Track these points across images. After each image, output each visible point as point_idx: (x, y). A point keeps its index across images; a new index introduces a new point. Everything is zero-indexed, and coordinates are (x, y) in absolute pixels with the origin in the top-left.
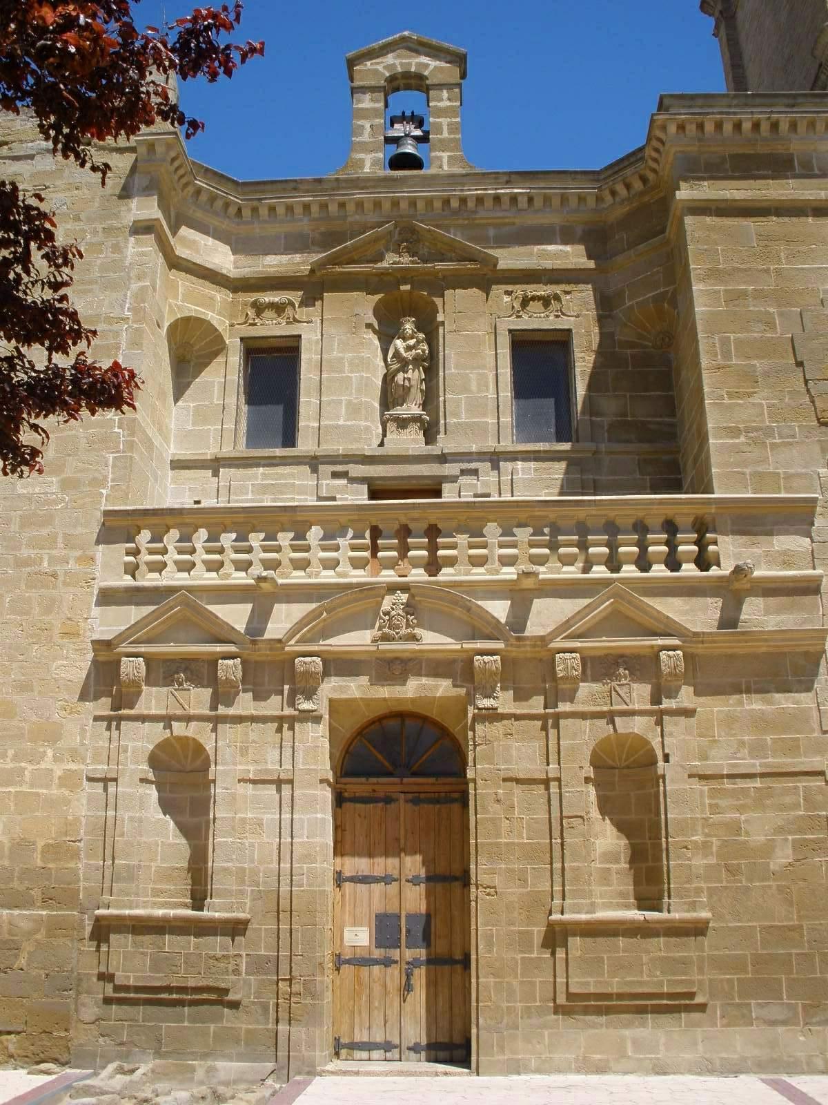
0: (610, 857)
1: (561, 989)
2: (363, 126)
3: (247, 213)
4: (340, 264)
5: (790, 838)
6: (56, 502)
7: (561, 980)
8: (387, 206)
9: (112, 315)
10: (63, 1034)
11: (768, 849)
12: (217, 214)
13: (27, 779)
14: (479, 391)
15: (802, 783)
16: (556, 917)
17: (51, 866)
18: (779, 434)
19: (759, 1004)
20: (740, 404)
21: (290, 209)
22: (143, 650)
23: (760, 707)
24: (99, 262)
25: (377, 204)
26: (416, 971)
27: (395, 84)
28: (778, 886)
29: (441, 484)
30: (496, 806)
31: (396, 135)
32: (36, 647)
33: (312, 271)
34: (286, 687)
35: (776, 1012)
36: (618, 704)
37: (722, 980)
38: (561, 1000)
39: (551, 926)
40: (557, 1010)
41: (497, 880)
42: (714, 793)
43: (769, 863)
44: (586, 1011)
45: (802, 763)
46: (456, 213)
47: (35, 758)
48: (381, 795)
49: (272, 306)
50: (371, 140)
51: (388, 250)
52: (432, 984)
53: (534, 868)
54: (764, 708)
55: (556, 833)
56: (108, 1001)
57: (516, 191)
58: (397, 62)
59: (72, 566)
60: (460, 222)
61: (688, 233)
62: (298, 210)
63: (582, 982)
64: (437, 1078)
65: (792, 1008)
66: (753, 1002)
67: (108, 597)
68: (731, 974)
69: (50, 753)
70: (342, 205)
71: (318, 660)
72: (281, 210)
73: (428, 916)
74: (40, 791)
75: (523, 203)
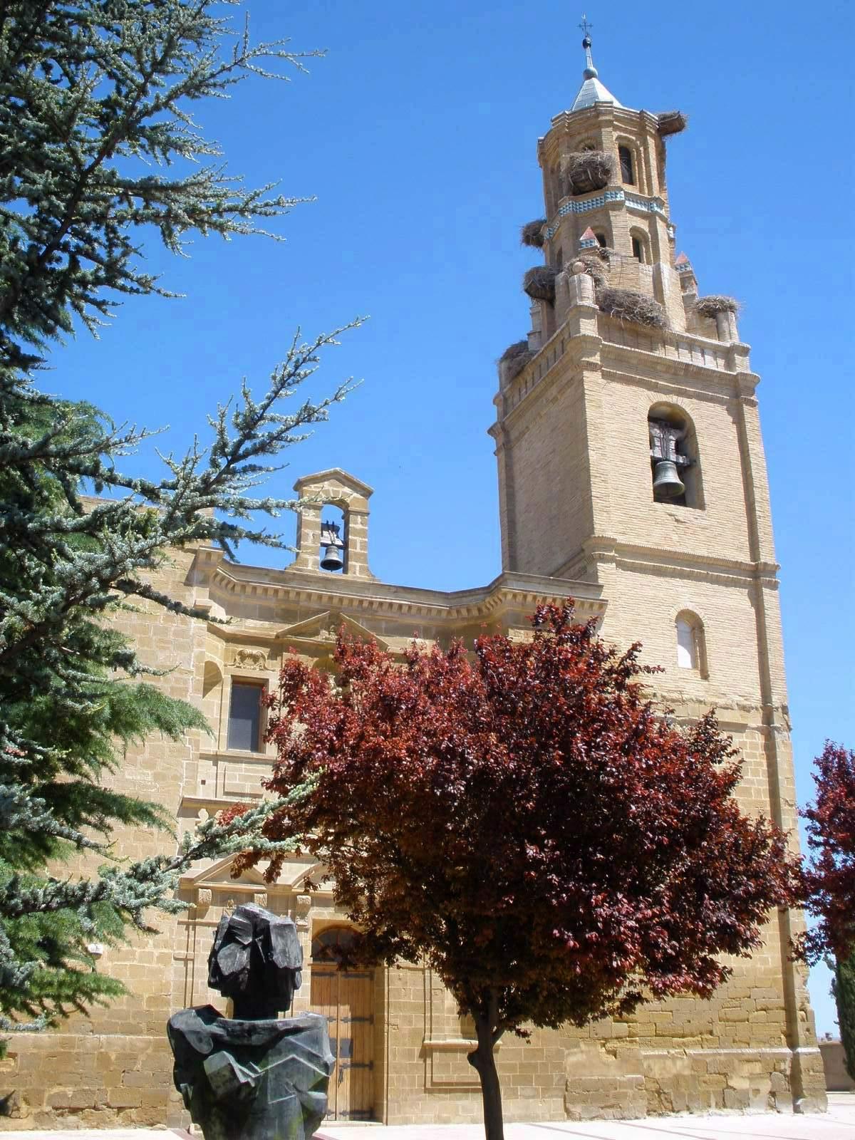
0: (450, 1011)
1: (428, 1080)
3: (238, 589)
4: (296, 635)
6: (151, 787)
7: (429, 1075)
8: (325, 600)
10: (164, 1108)
12: (221, 588)
16: (427, 1042)
22: (211, 885)
24: (173, 629)
25: (320, 597)
26: (345, 1071)
30: (399, 982)
33: (277, 637)
34: (290, 911)
35: (529, 1092)
38: (429, 1085)
39: (424, 1046)
40: (426, 1091)
41: (398, 1022)
44: (440, 1091)
46: (364, 610)
48: (329, 971)
49: (251, 656)
51: (322, 628)
52: (353, 1078)
55: (428, 996)
60: (367, 616)
62: (271, 593)
63: (439, 1076)
65: (537, 1090)
69: (151, 942)
70: (298, 594)
72: (259, 591)
73: (352, 1040)
74: (146, 965)
75: (405, 609)
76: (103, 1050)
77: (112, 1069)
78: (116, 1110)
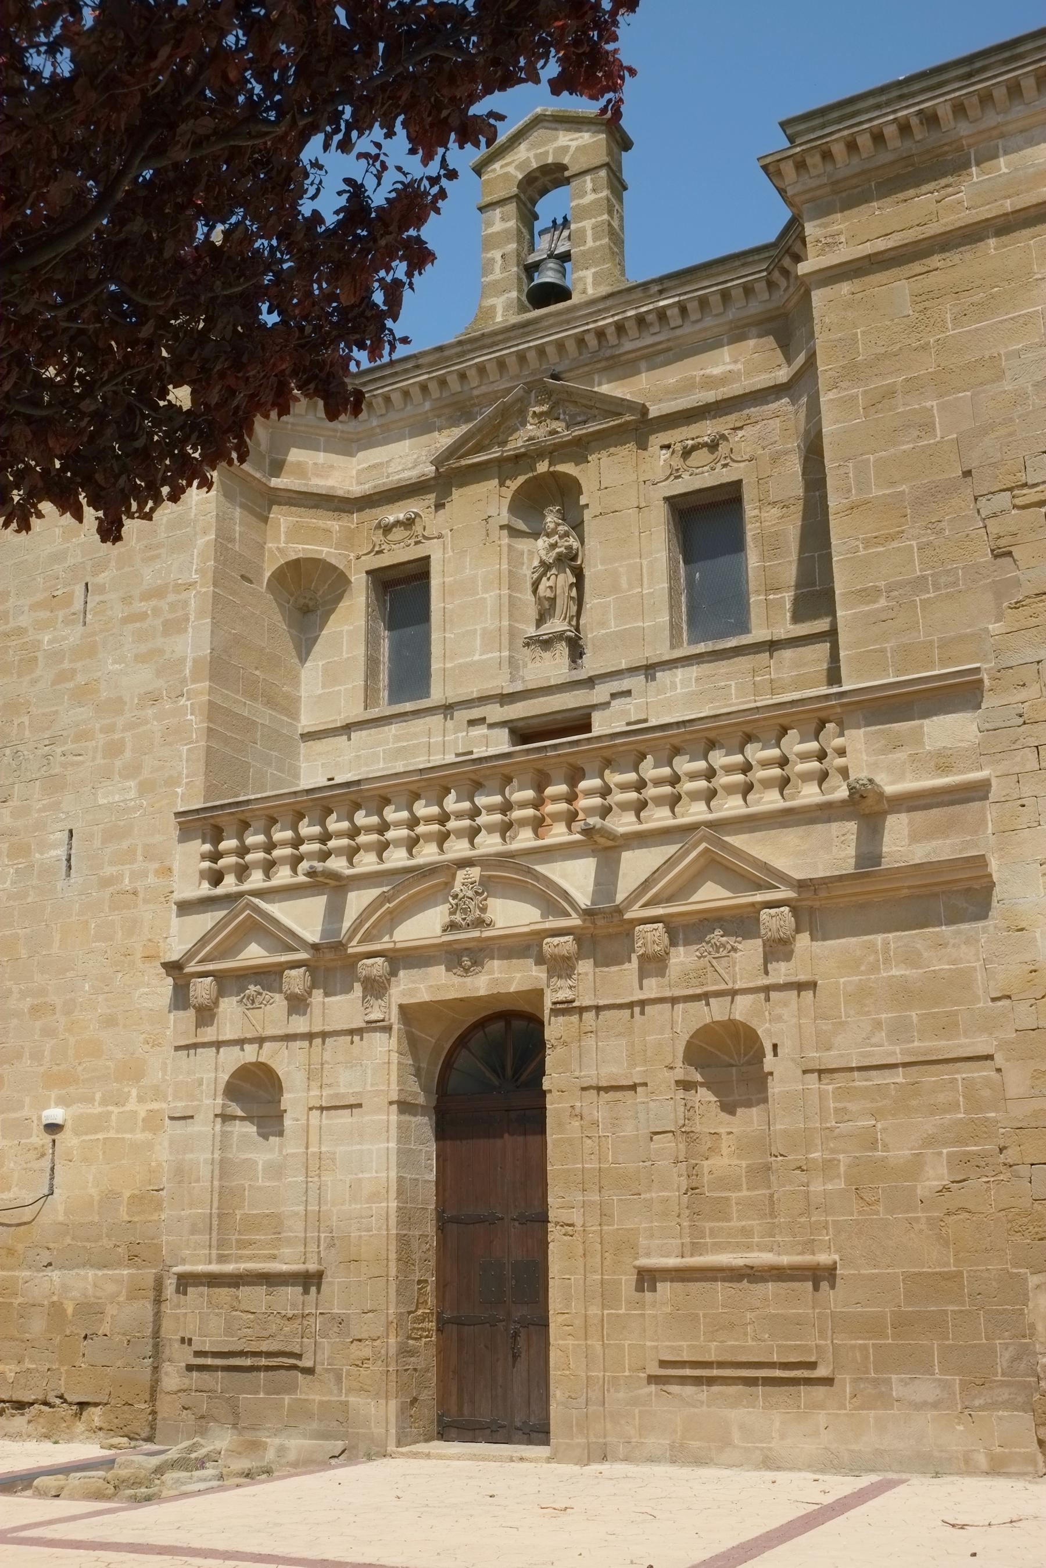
2: (493, 259)
5: (945, 1151)
9: (180, 581)
11: (914, 1168)
13: (114, 1124)
14: (631, 587)
15: (964, 1073)
17: (136, 1219)
18: (933, 585)
19: (902, 1380)
20: (879, 554)
21: (406, 393)
23: (902, 972)
27: (538, 184)
28: (928, 1218)
29: (589, 716)
31: (537, 259)
32: (120, 975)
35: (925, 1389)
36: (715, 982)
37: (853, 1347)
42: (842, 1093)
43: (916, 1186)
45: (960, 1046)
47: (119, 1101)
49: (398, 523)
50: (503, 275)
53: (621, 1200)
54: (907, 973)
56: (190, 1368)
57: (662, 303)
58: (531, 154)
59: (151, 880)
61: (816, 322)
62: (416, 392)
64: (512, 1464)
66: (894, 1377)
67: (185, 907)
68: (865, 1339)
70: (462, 376)
71: (380, 960)
76: (55, 1298)
77: (68, 1333)
78: (75, 1407)
